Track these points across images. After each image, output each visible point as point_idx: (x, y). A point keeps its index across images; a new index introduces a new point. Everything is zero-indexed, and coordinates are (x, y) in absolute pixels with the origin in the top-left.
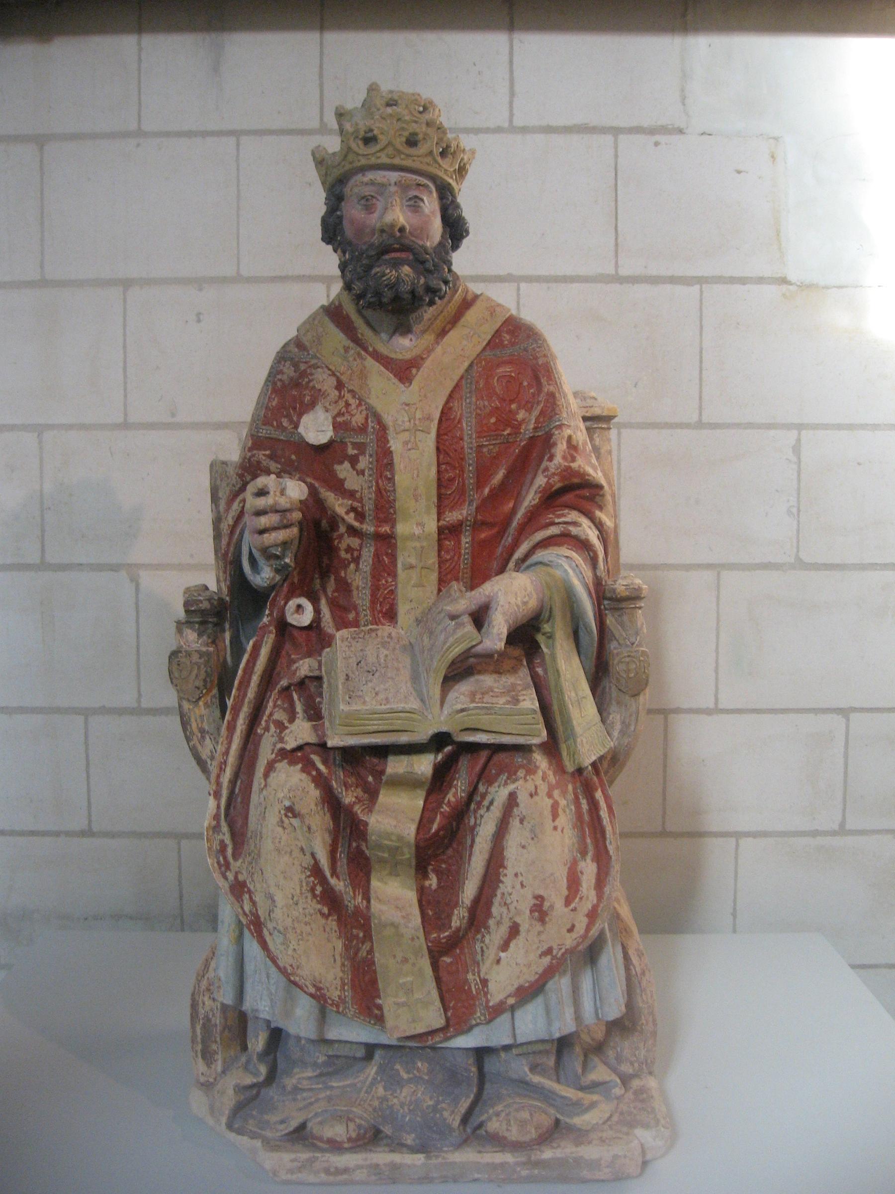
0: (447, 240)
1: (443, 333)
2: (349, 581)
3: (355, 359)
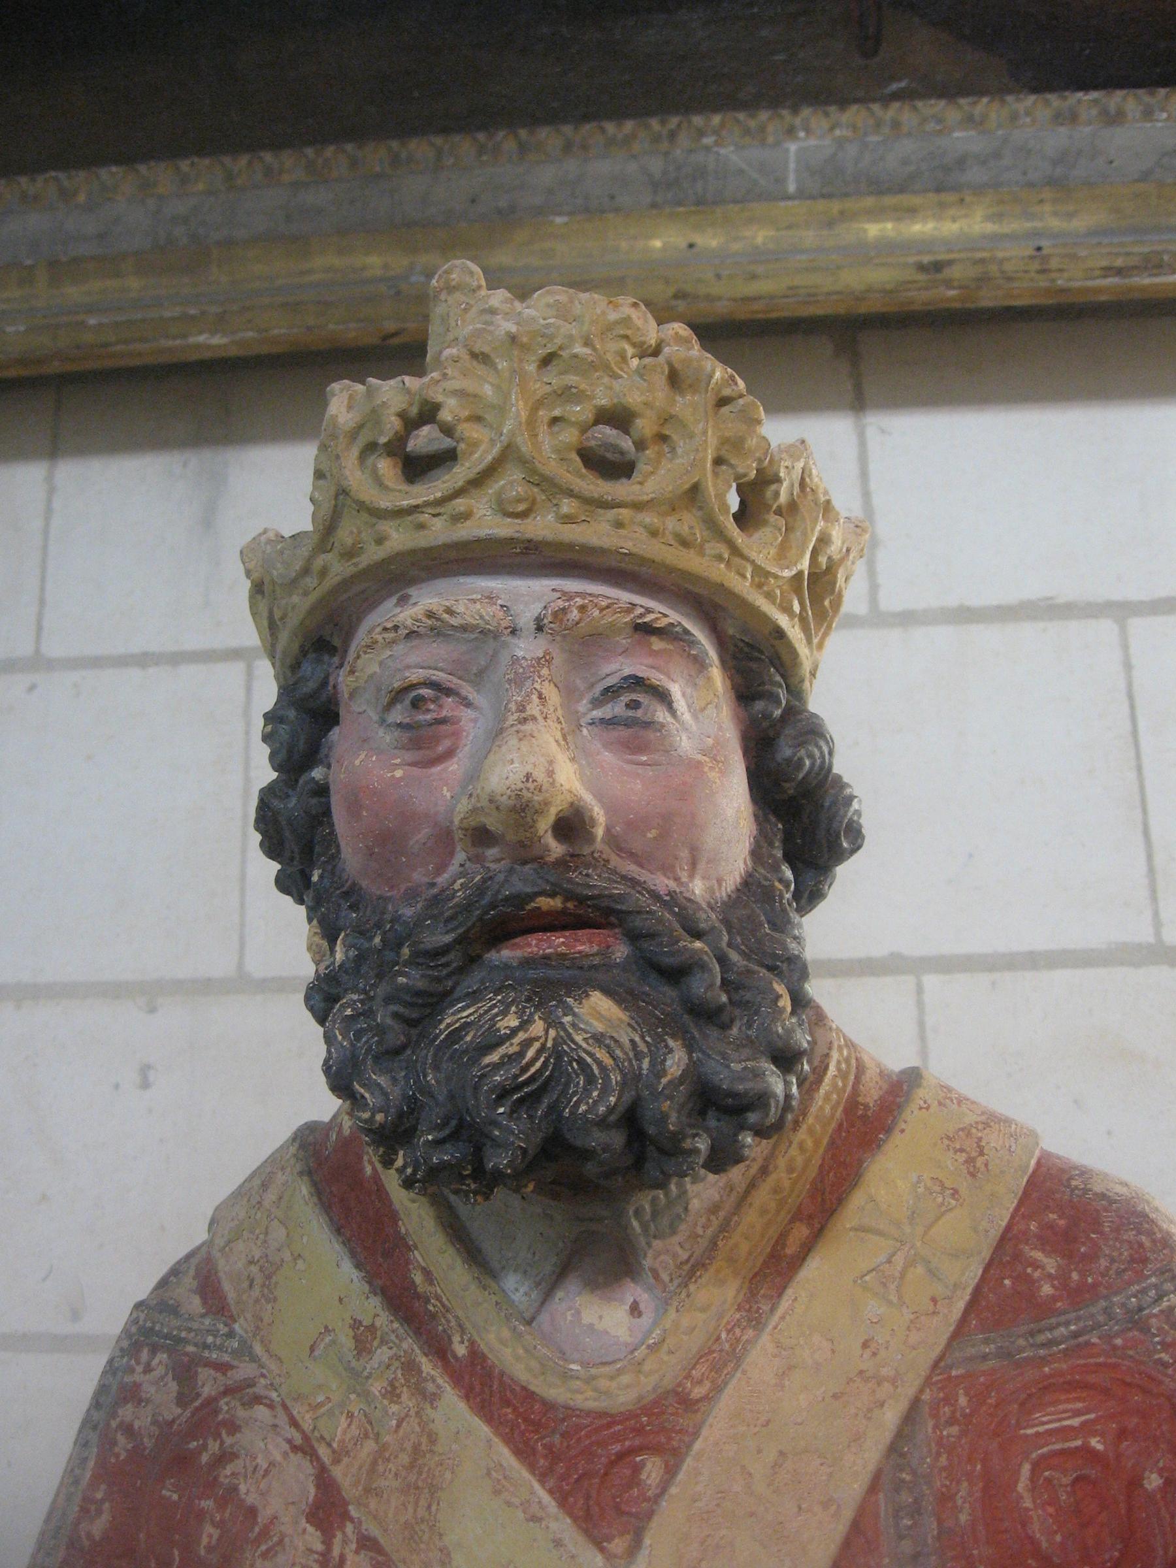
0: (776, 868)
1: (776, 1268)
3: (392, 1393)
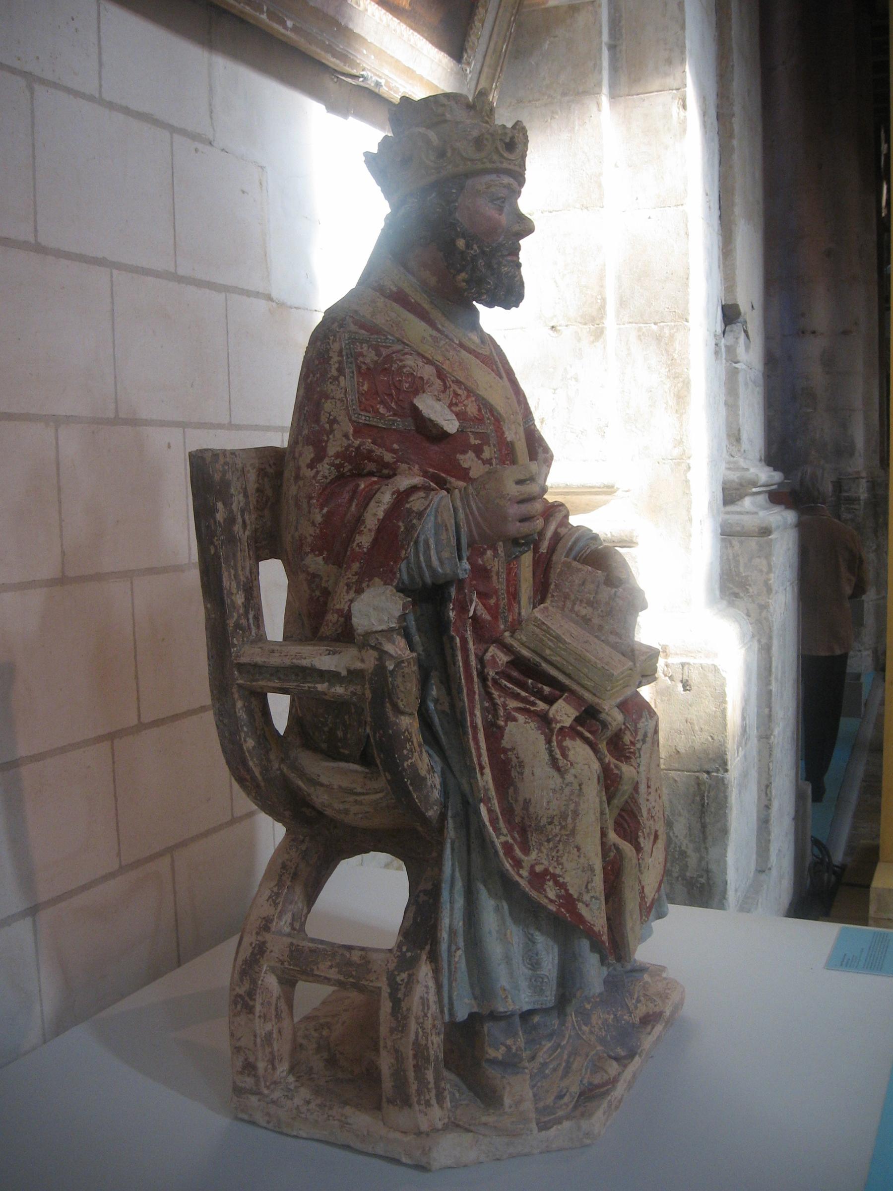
2: (489, 567)
